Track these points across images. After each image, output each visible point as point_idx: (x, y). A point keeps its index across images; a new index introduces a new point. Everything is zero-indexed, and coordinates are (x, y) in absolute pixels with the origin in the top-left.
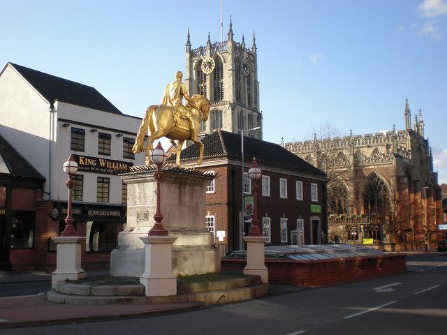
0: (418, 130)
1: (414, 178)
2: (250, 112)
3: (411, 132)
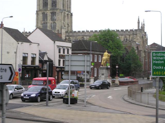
1: (140, 49)
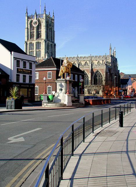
0: (114, 55)
1: (112, 73)
2: (51, 43)
3: (111, 56)
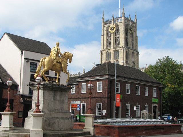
2: (133, 51)
